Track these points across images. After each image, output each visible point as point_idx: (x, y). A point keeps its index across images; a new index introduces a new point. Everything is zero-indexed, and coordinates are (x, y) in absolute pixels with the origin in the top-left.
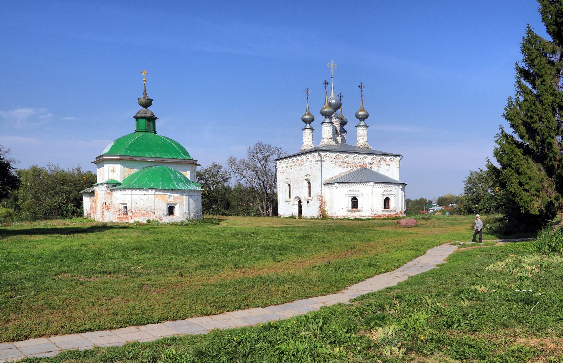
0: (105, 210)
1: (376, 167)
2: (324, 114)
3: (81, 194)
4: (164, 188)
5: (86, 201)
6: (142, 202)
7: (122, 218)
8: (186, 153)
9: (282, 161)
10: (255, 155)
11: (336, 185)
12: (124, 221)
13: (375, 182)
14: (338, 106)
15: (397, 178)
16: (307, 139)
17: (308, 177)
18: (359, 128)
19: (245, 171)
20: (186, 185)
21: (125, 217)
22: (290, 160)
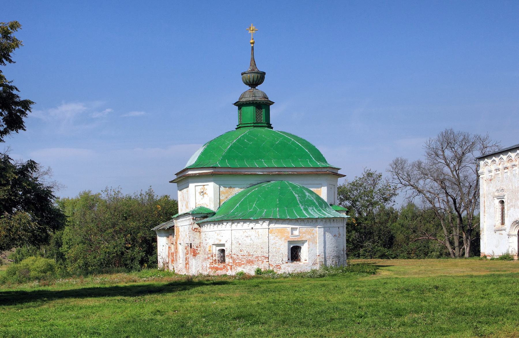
0: (190, 256)
3: (155, 233)
4: (283, 217)
5: (162, 242)
6: (248, 241)
7: (217, 269)
8: (320, 157)
10: (440, 153)
12: (220, 272)
19: (421, 182)
20: (319, 211)
21: (221, 266)
22: (504, 157)
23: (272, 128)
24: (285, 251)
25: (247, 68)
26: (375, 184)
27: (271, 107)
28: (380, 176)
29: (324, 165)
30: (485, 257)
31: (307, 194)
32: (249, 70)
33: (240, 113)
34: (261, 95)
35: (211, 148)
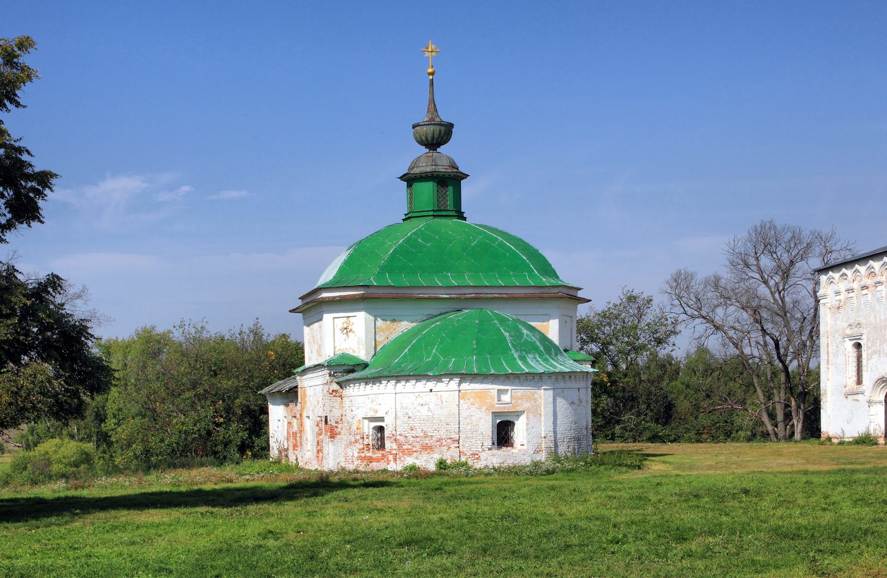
0: (325, 438)
4: (484, 371)
5: (277, 413)
6: (424, 412)
7: (371, 460)
8: (547, 269)
10: (752, 261)
19: (720, 311)
20: (546, 360)
21: (378, 454)
22: (862, 269)
23: (465, 219)
24: (487, 428)
25: (423, 116)
26: (640, 315)
27: (463, 183)
28: (650, 301)
29: (554, 282)
30: (829, 439)
31: (525, 331)
32: (426, 119)
33: (411, 194)
34: (446, 163)
35: (360, 253)
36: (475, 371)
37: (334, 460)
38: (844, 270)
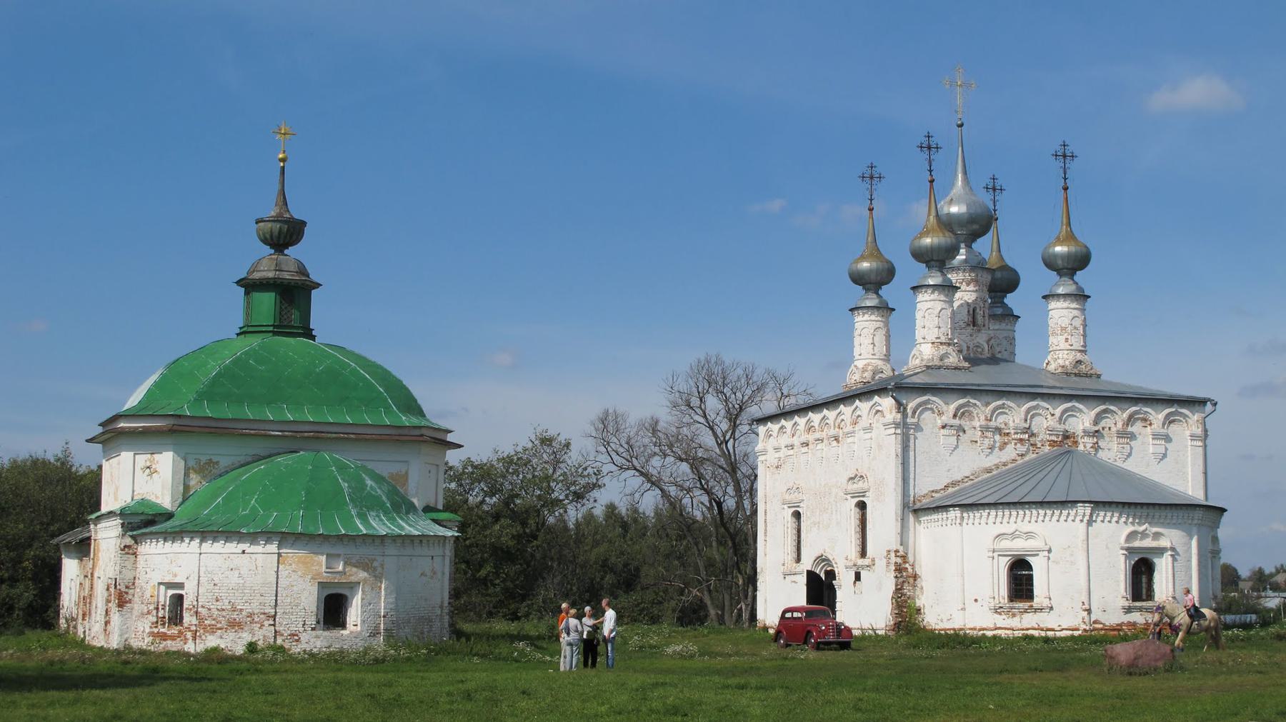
0: (113, 606)
1: (1115, 447)
2: (922, 256)
4: (311, 530)
5: (70, 568)
6: (234, 579)
7: (164, 637)
8: (411, 406)
9: (773, 427)
10: (695, 402)
11: (954, 513)
12: (172, 645)
13: (1098, 505)
14: (978, 225)
15: (1193, 490)
16: (866, 345)
17: (860, 485)
18: (1053, 304)
19: (656, 462)
20: (392, 520)
21: (174, 631)
22: (801, 421)
26: (556, 463)
27: (313, 292)
28: (568, 445)
29: (415, 421)
31: (369, 482)
32: (273, 213)
33: (248, 303)
34: (293, 267)
35: (176, 372)
36: (300, 529)
37: (121, 636)
38: (783, 422)
